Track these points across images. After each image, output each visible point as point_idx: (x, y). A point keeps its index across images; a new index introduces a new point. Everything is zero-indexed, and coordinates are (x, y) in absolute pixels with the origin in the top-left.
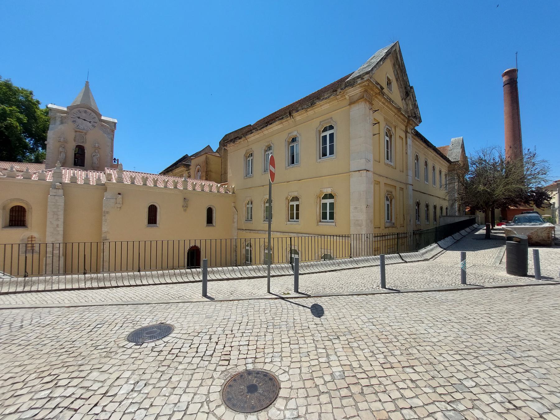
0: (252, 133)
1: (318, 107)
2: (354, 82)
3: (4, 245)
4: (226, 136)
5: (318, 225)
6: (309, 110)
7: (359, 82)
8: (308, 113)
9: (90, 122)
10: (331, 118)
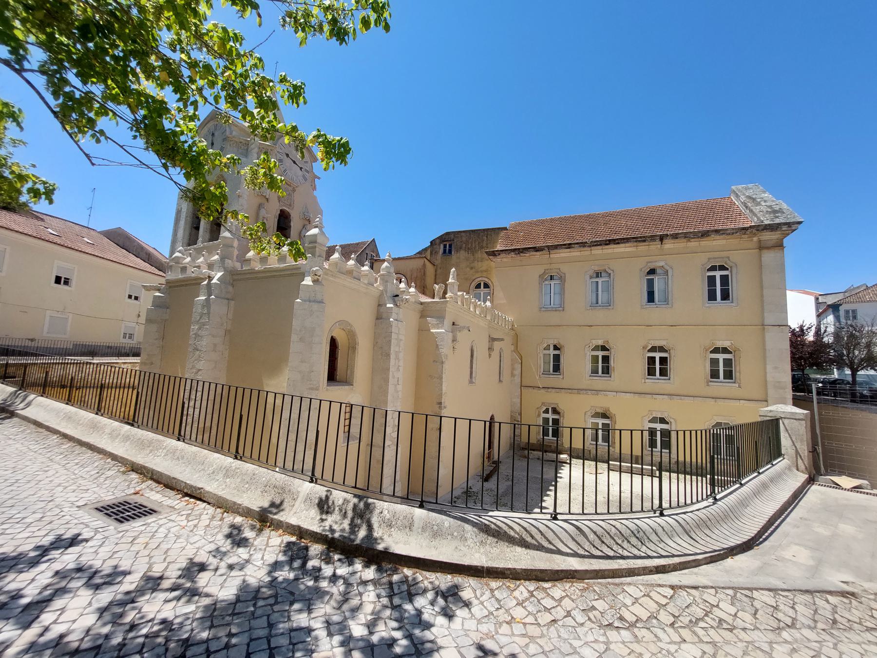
0: (569, 248)
1: (711, 240)
2: (778, 227)
3: (524, 390)
4: (448, 234)
5: (708, 385)
6: (693, 240)
7: (784, 229)
8: (689, 243)
9: (301, 168)
10: (728, 258)
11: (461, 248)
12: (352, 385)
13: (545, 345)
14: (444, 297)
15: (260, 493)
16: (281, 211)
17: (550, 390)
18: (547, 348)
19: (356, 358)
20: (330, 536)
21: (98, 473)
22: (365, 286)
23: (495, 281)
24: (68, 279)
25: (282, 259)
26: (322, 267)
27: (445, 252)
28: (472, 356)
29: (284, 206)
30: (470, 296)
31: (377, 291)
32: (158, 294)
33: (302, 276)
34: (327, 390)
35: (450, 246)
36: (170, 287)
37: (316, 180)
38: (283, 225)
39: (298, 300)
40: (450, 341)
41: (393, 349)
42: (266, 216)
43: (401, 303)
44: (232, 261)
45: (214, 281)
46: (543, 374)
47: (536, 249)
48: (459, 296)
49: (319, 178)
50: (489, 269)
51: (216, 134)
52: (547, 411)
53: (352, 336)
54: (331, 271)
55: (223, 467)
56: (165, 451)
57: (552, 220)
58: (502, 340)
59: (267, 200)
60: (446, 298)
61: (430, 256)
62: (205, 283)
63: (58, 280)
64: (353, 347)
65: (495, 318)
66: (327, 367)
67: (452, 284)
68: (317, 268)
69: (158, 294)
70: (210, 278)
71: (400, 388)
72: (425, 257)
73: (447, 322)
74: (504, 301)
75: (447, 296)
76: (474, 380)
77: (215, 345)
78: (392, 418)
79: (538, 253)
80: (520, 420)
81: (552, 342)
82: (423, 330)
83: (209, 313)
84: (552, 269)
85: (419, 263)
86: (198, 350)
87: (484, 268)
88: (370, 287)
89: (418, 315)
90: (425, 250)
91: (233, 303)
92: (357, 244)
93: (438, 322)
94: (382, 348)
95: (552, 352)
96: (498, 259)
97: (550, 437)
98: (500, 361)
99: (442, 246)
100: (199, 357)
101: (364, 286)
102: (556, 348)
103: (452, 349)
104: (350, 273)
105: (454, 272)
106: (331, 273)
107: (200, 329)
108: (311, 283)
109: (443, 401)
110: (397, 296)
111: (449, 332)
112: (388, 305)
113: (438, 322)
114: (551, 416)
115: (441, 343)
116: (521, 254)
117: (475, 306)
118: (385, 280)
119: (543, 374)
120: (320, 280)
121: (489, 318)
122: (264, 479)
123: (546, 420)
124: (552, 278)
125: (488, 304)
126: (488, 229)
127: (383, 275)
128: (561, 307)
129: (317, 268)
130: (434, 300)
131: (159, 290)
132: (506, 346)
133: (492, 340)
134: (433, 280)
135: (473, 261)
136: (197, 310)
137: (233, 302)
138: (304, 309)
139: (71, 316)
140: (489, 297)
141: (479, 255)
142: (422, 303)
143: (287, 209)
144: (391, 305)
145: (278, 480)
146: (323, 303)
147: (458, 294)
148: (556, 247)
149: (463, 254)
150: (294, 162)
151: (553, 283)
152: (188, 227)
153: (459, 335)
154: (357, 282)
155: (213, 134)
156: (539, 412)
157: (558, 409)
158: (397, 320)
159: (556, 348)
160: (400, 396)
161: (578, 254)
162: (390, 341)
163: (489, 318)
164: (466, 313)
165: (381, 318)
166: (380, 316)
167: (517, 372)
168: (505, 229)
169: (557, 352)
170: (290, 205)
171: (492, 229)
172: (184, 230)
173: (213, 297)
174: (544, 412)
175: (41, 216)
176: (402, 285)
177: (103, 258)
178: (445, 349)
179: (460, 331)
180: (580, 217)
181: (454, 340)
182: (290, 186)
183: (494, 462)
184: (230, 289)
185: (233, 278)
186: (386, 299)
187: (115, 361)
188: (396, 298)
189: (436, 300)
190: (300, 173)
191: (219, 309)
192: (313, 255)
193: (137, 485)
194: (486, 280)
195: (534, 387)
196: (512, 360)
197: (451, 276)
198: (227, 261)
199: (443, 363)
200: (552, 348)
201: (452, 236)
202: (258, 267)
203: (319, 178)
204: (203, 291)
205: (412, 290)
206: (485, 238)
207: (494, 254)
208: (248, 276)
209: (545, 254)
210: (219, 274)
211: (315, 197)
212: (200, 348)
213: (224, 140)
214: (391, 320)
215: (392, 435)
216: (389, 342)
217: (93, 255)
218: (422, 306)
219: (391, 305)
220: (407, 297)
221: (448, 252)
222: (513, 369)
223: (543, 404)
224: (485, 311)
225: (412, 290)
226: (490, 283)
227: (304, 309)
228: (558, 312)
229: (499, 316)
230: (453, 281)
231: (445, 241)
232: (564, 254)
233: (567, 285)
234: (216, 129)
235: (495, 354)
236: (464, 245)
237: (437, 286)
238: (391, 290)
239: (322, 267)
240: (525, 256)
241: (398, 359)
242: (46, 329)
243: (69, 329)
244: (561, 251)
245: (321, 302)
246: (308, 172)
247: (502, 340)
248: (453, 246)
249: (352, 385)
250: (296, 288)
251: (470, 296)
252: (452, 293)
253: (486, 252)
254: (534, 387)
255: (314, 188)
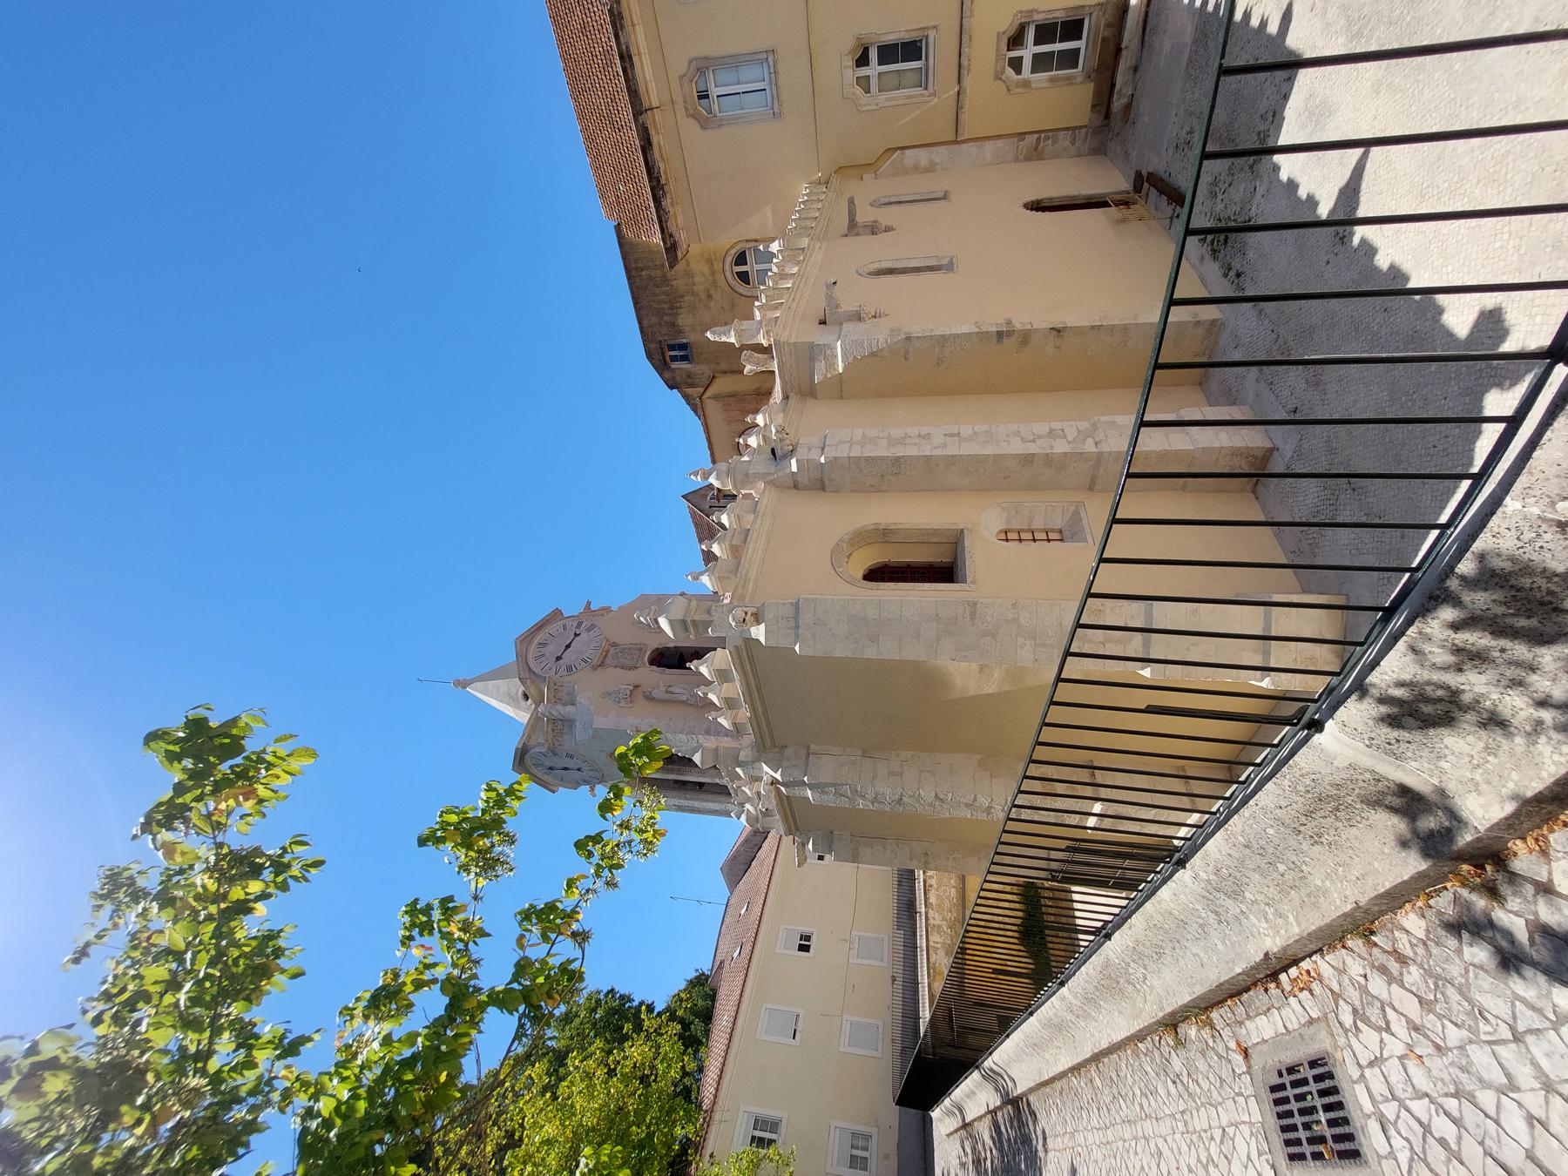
0: (630, 57)
4: (649, 356)
9: (576, 635)
11: (673, 324)
12: (962, 531)
13: (859, 91)
14: (766, 350)
15: (1317, 848)
16: (651, 663)
17: (965, 62)
18: (864, 83)
19: (908, 526)
20: (1091, 463)
21: (1174, 1082)
22: (759, 518)
23: (727, 240)
24: (802, 936)
25: (723, 676)
26: (731, 608)
27: (685, 358)
28: (891, 271)
29: (643, 658)
30: (762, 291)
31: (767, 493)
32: (810, 846)
33: (751, 642)
34: (974, 582)
35: (672, 348)
36: (797, 829)
37: (593, 607)
38: (674, 659)
39: (797, 648)
40: (861, 326)
41: (882, 451)
42: (663, 688)
43: (788, 442)
44: (740, 750)
45: (778, 776)
46: (926, 89)
47: (647, 146)
48: (763, 316)
49: (589, 603)
50: (706, 256)
51: (550, 765)
52: (1016, 64)
53: (861, 538)
54: (736, 588)
55: (1206, 894)
56: (1132, 964)
57: (581, 117)
58: (851, 202)
59: (636, 687)
60: (770, 345)
61: (698, 386)
62: (783, 789)
63: (804, 948)
64: (884, 535)
65: (805, 228)
66: (926, 585)
67: (739, 335)
68: (731, 620)
69: (810, 846)
70: (774, 782)
71: (966, 430)
72: (700, 398)
73: (820, 337)
74: (768, 211)
75: (765, 343)
76: (945, 261)
77: (892, 773)
78: (1034, 441)
79: (655, 140)
80: (1036, 136)
81: (851, 73)
82: (841, 389)
83: (835, 785)
84: (685, 97)
85: (712, 408)
86: (901, 799)
87: (706, 270)
88: (761, 507)
89: (810, 402)
90: (686, 397)
91: (813, 747)
92: (696, 525)
93: (822, 358)
94: (882, 476)
95: (874, 69)
96: (682, 237)
97: (1080, 44)
98: (900, 202)
99: (675, 365)
100: (913, 797)
101: (759, 522)
102: (862, 61)
103: (878, 320)
104: (736, 551)
105: (713, 333)
106: (740, 589)
107: (863, 797)
108: (762, 626)
109: (995, 329)
110: (773, 451)
111: (841, 331)
112: (794, 468)
113: (822, 358)
114: (1028, 51)
115: (866, 345)
116: (663, 181)
117: (783, 276)
118: (746, 479)
119: (926, 89)
120: (754, 610)
121: (804, 242)
122: (1270, 831)
123: (1041, 63)
124: (703, 96)
125: (775, 247)
126: (626, 268)
127: (735, 485)
128: (766, 58)
129: (731, 620)
130: (777, 371)
131: (804, 845)
132: (866, 191)
133: (853, 227)
134: (737, 377)
135: (696, 295)
136: (829, 800)
137: (812, 746)
138: (813, 635)
139: (854, 933)
140: (761, 248)
141: (680, 284)
142: (786, 397)
143: (648, 654)
144: (794, 462)
145: (1283, 804)
146: (798, 603)
147: (759, 318)
148: (633, 93)
149: (684, 319)
150: (568, 646)
151: (715, 92)
152: (703, 796)
153: (847, 307)
154: (753, 535)
155: (551, 768)
156: (1018, 85)
157: (1011, 32)
158: (823, 449)
159: (862, 61)
160: (984, 428)
161: (639, 30)
162: (867, 459)
163: (804, 242)
164: (798, 295)
165: (822, 481)
166: (819, 483)
167: (923, 156)
168: (618, 228)
169: (873, 55)
170: (640, 650)
171: (624, 259)
172: (707, 801)
173: (805, 779)
174: (1018, 71)
175: (718, 963)
176: (753, 441)
177: (767, 893)
178: (878, 335)
179: (837, 306)
180: (561, 41)
181: (858, 317)
182: (608, 651)
183: (1137, 188)
184: (789, 751)
185: (769, 745)
186: (781, 474)
187: (922, 884)
188: (779, 452)
189: (775, 367)
190: (584, 636)
191: (826, 769)
192: (708, 624)
193: (1218, 1040)
194: (729, 259)
195: (959, 107)
196: (894, 175)
197: (724, 339)
198: (742, 755)
199: (909, 339)
200: (863, 71)
201: (653, 346)
202: (744, 713)
203: (589, 603)
204: (797, 792)
205: (760, 419)
206: (644, 273)
207: (672, 248)
208: (764, 725)
209: (654, 121)
210: (766, 768)
211: (621, 608)
212: (897, 797)
213: (555, 754)
214: (822, 460)
215: (1070, 439)
216: (870, 461)
217: (764, 905)
218: (792, 395)
219: (794, 462)
220: (774, 431)
221: (685, 351)
222: (917, 169)
223: (998, 76)
224: (792, 252)
225: (760, 419)
226: (733, 252)
227: (813, 635)
228: (780, 67)
229: (799, 219)
230: (732, 333)
231: (665, 362)
232: (645, 69)
233: (714, 51)
234: (542, 765)
235: (885, 216)
236: (666, 318)
237: (748, 368)
238: (763, 465)
239: (731, 608)
240: (665, 173)
241: (904, 438)
242: (878, 963)
243: (873, 1021)
244: (640, 79)
245: (796, 606)
246: (578, 626)
247: (851, 202)
248: (671, 342)
249: (962, 531)
250: (777, 655)
251: (762, 291)
252: (758, 333)
253: (671, 267)
254: (959, 107)
255: (607, 609)
